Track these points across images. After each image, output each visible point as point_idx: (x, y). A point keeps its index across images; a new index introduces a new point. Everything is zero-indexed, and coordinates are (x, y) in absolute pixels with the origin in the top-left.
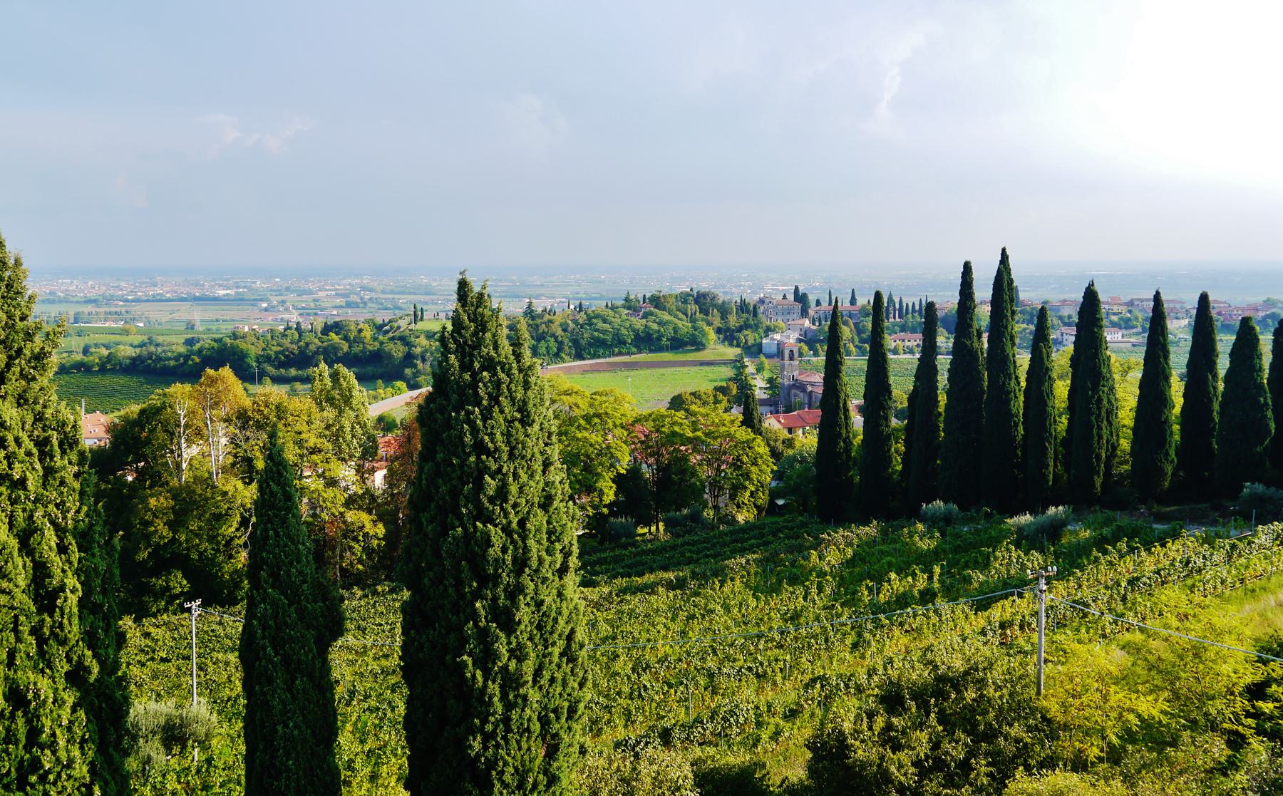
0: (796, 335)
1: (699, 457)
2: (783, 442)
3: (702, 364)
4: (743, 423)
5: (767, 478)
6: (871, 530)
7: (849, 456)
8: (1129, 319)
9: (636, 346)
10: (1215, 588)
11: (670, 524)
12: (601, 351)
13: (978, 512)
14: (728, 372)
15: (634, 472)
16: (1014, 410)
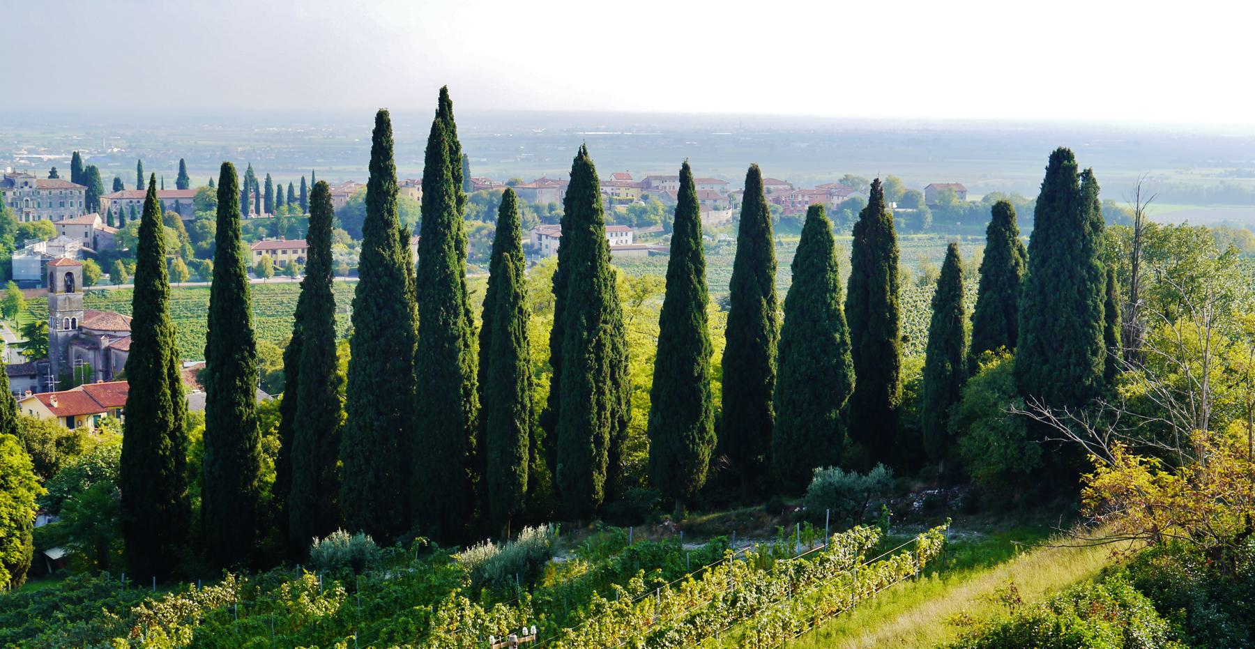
2: (58, 443)
5: (29, 512)
6: (226, 591)
7: (181, 463)
8: (644, 211)
10: (774, 637)
13: (407, 546)
16: (464, 368)
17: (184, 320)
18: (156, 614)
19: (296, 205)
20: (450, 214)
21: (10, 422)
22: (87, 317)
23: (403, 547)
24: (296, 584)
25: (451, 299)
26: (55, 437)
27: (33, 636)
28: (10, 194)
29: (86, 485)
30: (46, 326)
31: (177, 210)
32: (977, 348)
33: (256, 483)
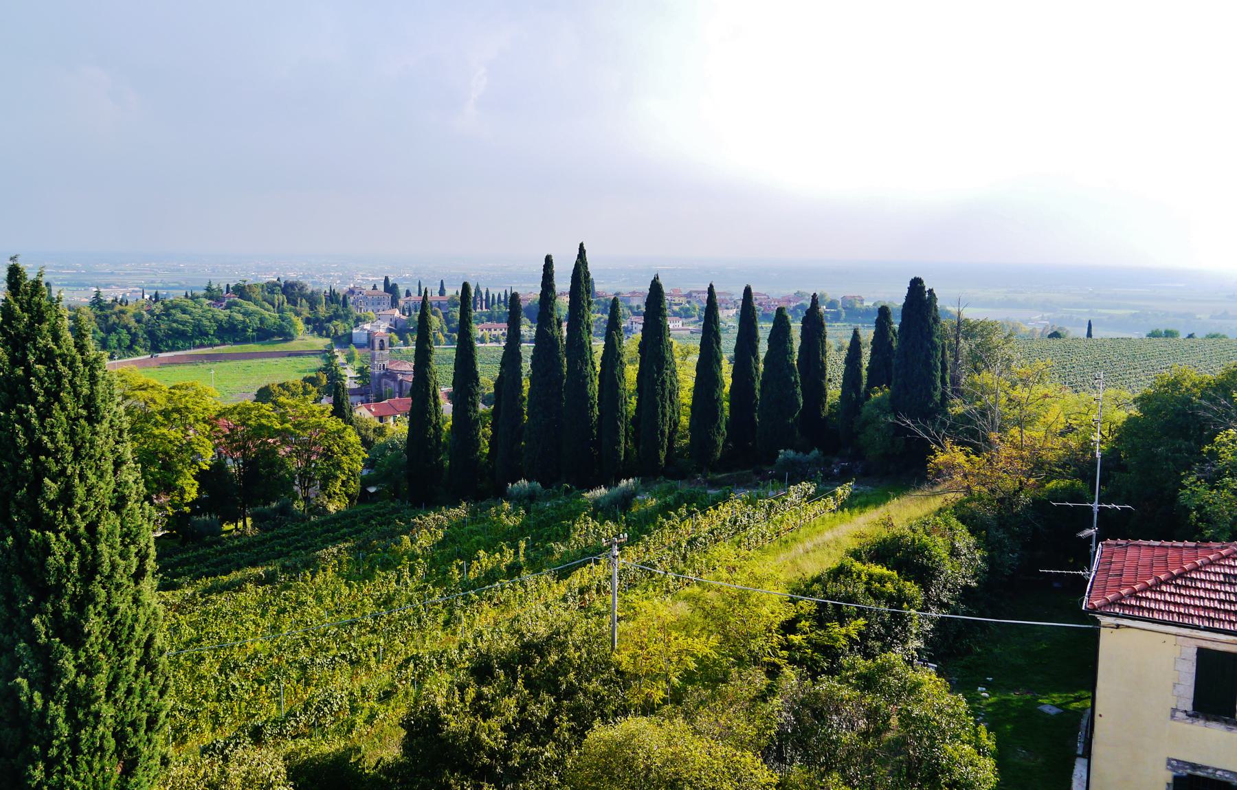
0: (387, 325)
3: (291, 354)
4: (333, 413)
6: (461, 511)
7: (439, 442)
8: (688, 309)
12: (180, 343)
13: (558, 488)
14: (317, 362)
15: (218, 467)
16: (591, 393)
32: (870, 385)
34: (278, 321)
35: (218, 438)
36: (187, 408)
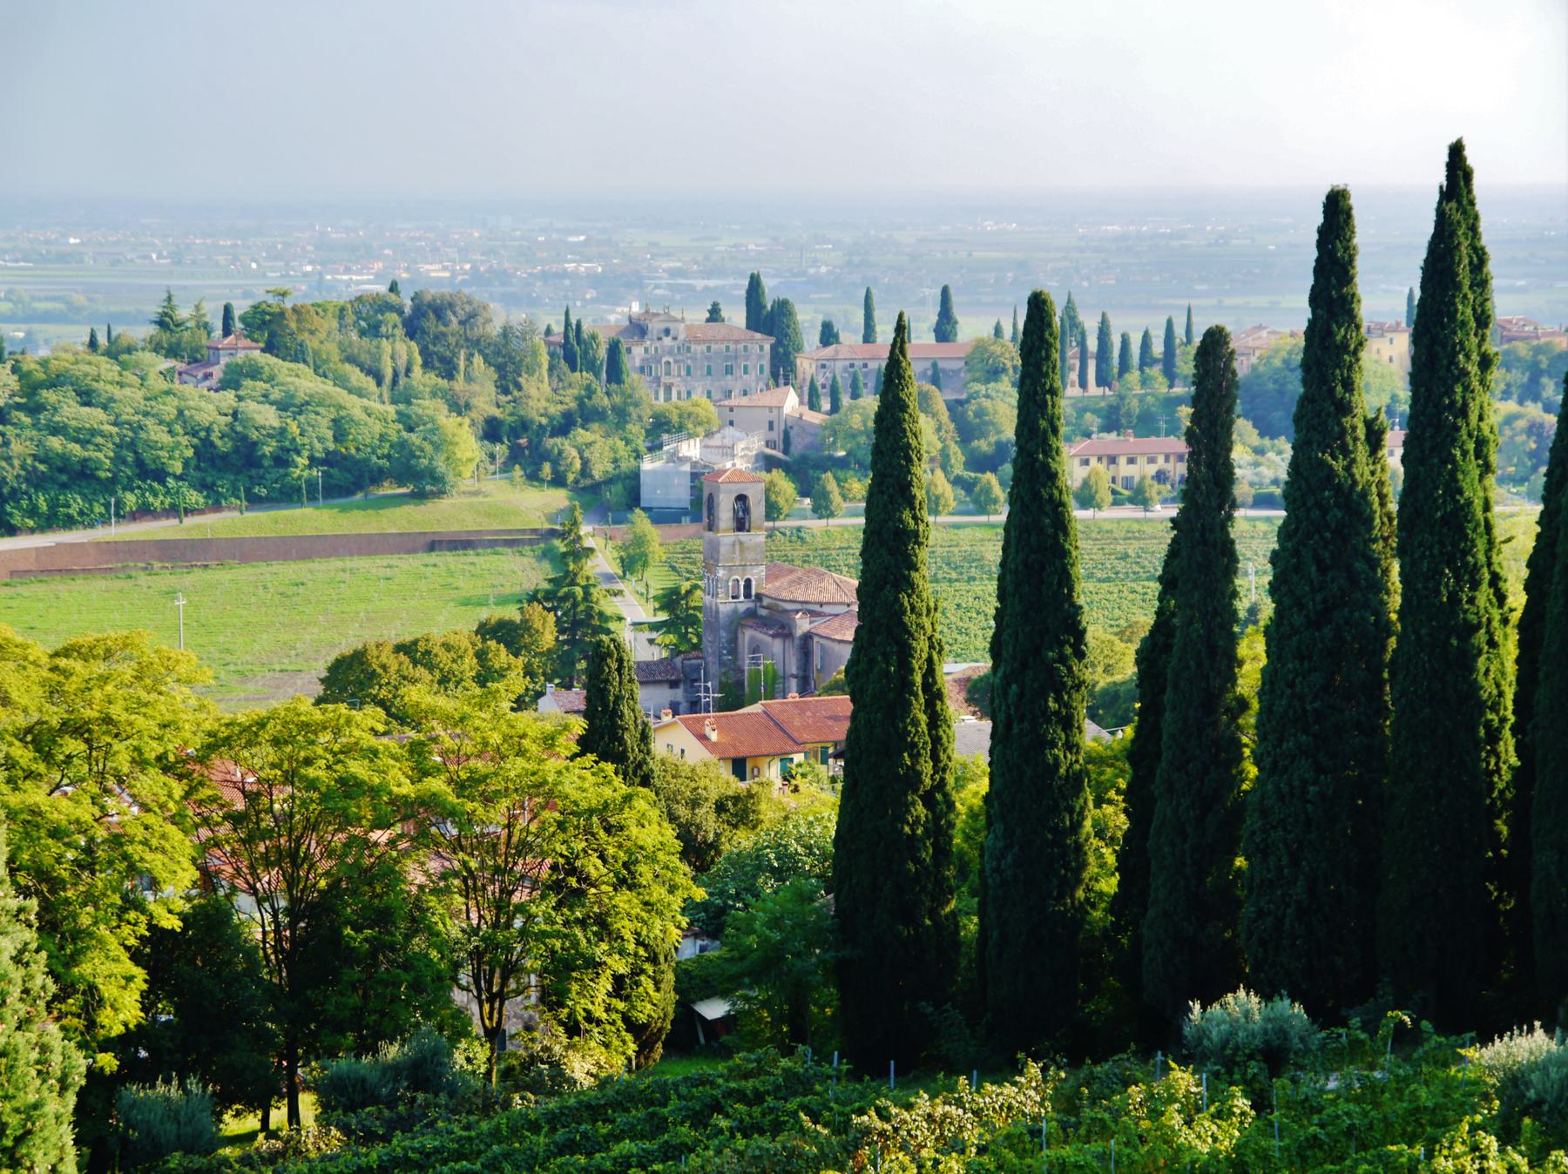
1: (434, 865)
2: (720, 807)
3: (434, 545)
4: (586, 744)
5: (670, 932)
6: (1026, 1093)
7: (943, 852)
9: (204, 486)
11: (341, 1099)
12: (76, 503)
13: (1371, 1026)
14: (530, 573)
15: (209, 921)
16: (1488, 688)
17: (945, 585)
18: (896, 1130)
19: (1155, 371)
20: (1466, 388)
21: (639, 766)
22: (771, 576)
23: (1364, 1028)
24: (1158, 1088)
25: (1465, 553)
26: (714, 796)
27: (677, 1159)
28: (638, 351)
29: (767, 885)
30: (698, 593)
31: (935, 380)
33: (1080, 894)
34: (395, 431)
35: (206, 821)
36: (108, 720)
